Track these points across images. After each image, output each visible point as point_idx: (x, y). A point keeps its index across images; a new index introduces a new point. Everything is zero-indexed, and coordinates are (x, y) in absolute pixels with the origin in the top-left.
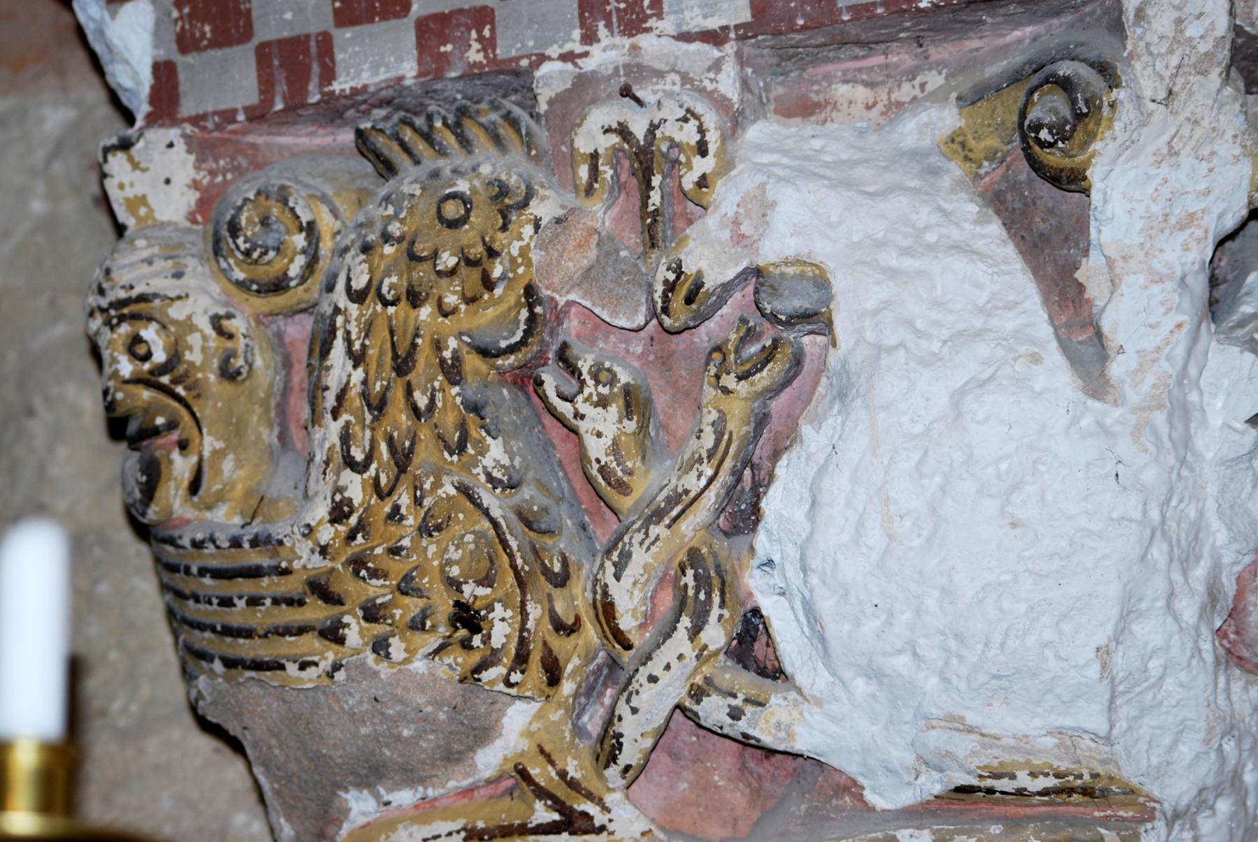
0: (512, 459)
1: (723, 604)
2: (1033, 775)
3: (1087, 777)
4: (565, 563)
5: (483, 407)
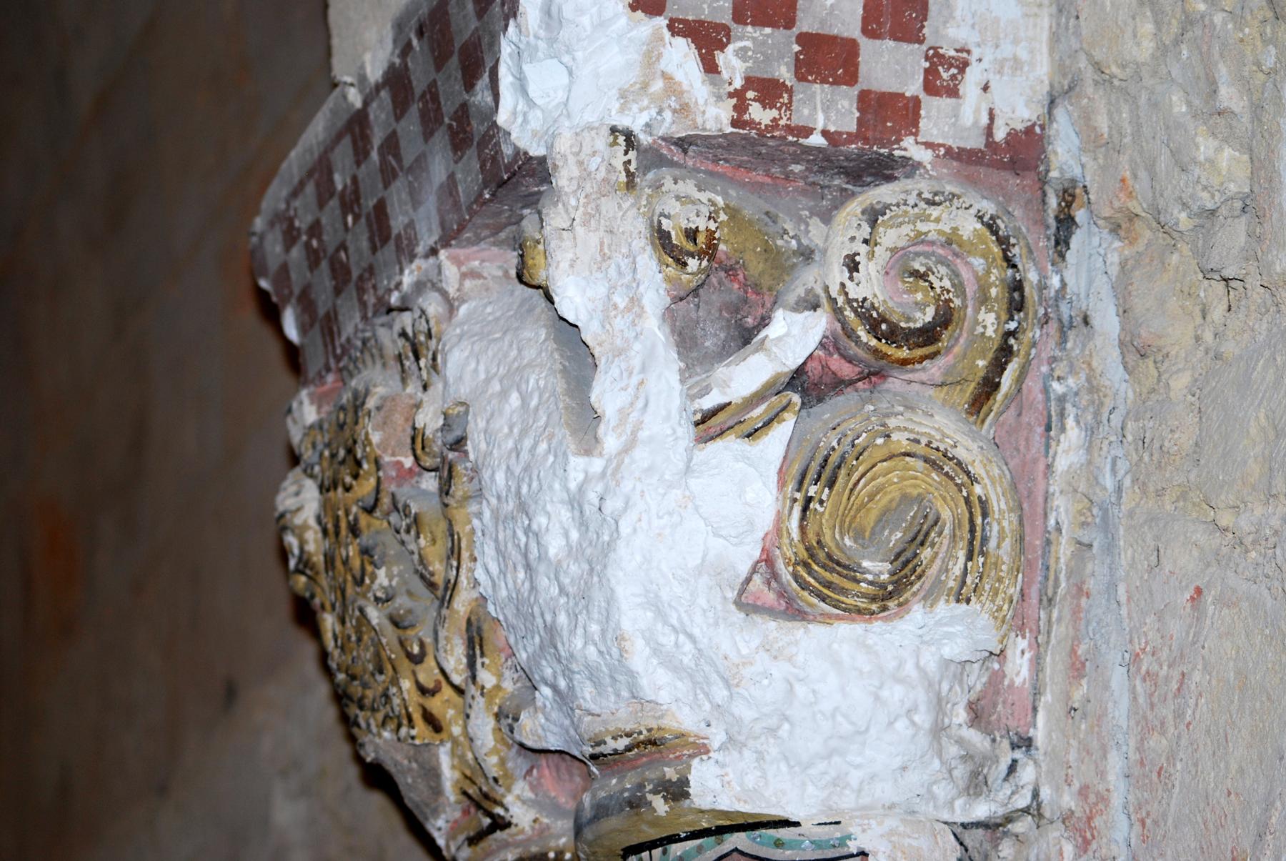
0: (390, 581)
1: (482, 655)
2: (614, 738)
3: (645, 732)
4: (422, 645)
5: (373, 548)
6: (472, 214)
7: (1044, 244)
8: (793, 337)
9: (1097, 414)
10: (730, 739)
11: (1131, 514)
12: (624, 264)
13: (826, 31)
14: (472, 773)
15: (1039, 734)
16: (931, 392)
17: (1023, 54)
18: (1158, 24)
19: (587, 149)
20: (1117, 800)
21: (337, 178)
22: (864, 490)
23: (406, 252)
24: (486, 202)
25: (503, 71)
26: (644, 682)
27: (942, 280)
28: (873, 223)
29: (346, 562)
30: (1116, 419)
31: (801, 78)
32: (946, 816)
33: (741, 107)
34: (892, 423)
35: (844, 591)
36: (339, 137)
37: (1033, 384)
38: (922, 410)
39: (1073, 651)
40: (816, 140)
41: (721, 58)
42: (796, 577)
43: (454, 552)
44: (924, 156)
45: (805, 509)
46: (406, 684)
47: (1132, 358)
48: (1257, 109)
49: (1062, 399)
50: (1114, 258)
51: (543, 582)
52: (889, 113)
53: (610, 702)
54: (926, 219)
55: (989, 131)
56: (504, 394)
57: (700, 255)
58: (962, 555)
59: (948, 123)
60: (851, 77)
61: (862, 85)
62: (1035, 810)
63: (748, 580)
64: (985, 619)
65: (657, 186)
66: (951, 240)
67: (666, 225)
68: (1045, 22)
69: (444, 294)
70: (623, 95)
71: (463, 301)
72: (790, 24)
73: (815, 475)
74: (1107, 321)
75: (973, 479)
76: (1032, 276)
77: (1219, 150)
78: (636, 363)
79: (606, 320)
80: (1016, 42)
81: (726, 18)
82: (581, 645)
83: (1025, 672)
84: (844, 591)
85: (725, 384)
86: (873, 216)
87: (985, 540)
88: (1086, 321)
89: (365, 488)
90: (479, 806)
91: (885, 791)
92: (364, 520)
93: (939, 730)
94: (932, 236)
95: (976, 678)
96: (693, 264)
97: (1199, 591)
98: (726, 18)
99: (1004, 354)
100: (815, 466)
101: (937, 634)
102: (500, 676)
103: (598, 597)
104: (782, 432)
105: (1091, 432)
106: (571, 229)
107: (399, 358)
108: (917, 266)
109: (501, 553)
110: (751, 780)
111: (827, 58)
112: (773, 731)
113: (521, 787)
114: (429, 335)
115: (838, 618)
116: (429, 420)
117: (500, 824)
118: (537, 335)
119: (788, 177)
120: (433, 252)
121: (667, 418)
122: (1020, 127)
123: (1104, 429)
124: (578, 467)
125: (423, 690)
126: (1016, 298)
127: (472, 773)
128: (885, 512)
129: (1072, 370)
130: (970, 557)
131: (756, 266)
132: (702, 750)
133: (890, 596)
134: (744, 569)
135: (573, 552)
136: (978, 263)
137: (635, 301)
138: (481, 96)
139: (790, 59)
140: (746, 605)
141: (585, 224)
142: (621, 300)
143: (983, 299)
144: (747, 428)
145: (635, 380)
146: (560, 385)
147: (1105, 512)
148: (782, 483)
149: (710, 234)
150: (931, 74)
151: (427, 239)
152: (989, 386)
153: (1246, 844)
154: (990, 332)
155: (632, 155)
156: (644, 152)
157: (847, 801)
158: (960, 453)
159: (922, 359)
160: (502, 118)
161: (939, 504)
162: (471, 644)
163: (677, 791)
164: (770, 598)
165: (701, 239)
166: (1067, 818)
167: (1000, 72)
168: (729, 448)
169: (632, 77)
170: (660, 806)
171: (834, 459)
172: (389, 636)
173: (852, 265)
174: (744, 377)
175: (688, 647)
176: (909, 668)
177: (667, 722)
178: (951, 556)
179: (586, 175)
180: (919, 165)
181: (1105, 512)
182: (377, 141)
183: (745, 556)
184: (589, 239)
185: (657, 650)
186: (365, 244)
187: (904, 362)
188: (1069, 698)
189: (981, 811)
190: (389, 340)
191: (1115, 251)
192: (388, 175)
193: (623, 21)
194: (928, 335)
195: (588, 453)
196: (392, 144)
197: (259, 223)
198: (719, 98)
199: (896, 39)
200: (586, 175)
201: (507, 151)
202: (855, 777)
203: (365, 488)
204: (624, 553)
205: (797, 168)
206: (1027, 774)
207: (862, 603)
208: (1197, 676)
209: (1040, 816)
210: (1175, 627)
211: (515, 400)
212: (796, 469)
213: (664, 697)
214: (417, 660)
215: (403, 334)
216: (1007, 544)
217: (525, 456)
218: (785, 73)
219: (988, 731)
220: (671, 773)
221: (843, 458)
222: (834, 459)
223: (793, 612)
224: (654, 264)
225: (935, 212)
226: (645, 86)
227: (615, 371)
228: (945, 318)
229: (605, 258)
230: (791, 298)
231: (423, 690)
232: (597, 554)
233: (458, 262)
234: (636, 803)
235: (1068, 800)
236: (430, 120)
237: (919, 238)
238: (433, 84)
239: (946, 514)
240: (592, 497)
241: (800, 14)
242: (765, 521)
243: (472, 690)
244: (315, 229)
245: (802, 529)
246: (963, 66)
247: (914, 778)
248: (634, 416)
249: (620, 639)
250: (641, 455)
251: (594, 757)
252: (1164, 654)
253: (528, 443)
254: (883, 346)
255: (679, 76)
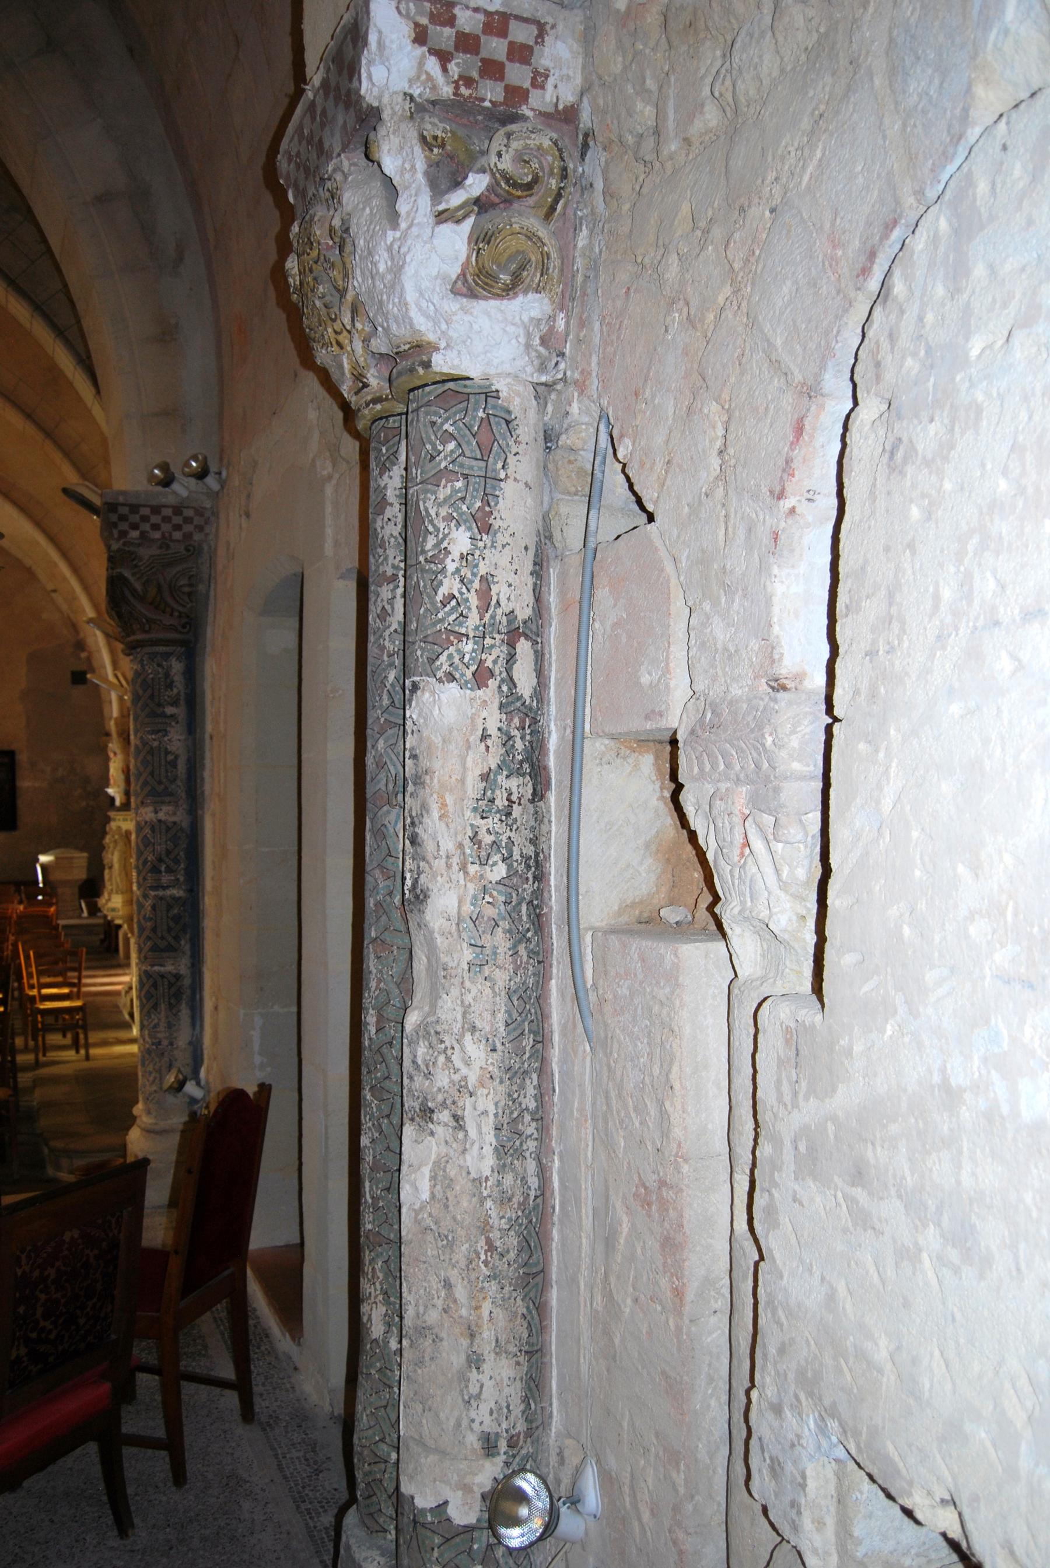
6: (353, 136)
7: (577, 154)
8: (476, 184)
9: (594, 224)
10: (448, 345)
11: (605, 261)
12: (409, 150)
13: (491, 58)
14: (356, 365)
15: (567, 351)
16: (529, 210)
17: (571, 73)
18: (624, 57)
19: (394, 102)
20: (594, 374)
21: (305, 131)
22: (501, 246)
23: (330, 158)
24: (357, 130)
25: (363, 70)
26: (415, 321)
27: (535, 165)
28: (508, 139)
29: (308, 283)
30: (601, 224)
31: (481, 77)
32: (530, 379)
33: (457, 88)
34: (513, 220)
35: (492, 287)
36: (305, 115)
37: (570, 212)
38: (525, 218)
39: (581, 318)
40: (487, 104)
41: (449, 67)
42: (474, 280)
43: (346, 276)
44: (529, 113)
45: (478, 253)
46: (330, 330)
47: (608, 198)
48: (661, 87)
49: (581, 218)
50: (603, 159)
51: (378, 283)
52: (516, 94)
53: (403, 331)
54: (529, 138)
55: (556, 105)
56: (364, 209)
57: (439, 147)
58: (538, 275)
59: (542, 100)
60: (502, 78)
61: (506, 82)
62: (564, 379)
63: (456, 282)
64: (546, 301)
65: (423, 119)
66: (539, 148)
67: (425, 133)
68: (580, 60)
69: (343, 172)
70: (410, 81)
71: (350, 175)
72: (477, 53)
73: (481, 239)
74: (599, 185)
75: (544, 245)
76: (571, 166)
77: (645, 107)
78: (413, 192)
79: (402, 174)
80: (568, 68)
81: (451, 49)
82: (392, 308)
83: (563, 327)
84: (492, 287)
85: (448, 202)
86: (508, 136)
87: (548, 269)
88: (591, 185)
89: (314, 254)
90: (358, 379)
91: (507, 368)
92: (314, 266)
93: (528, 346)
94: (532, 146)
95: (544, 328)
96: (436, 150)
97: (629, 289)
98: (451, 49)
99: (559, 196)
100: (482, 236)
101: (531, 306)
102: (364, 325)
103: (398, 288)
104: (470, 221)
105: (591, 231)
106: (388, 135)
107: (327, 201)
108: (526, 158)
109: (362, 273)
110: (456, 362)
111: (492, 69)
112: (464, 342)
113: (373, 371)
114: (337, 189)
115: (490, 298)
116: (336, 222)
117: (366, 385)
118: (377, 184)
119: (476, 121)
120: (339, 155)
121: (425, 215)
122: (569, 104)
123: (596, 228)
124: (391, 235)
125: (336, 332)
126: (564, 174)
127: (356, 365)
128: (510, 256)
129: (586, 206)
130: (542, 275)
131: (462, 156)
132: (437, 349)
133: (510, 289)
134: (454, 277)
135: (389, 270)
136: (550, 158)
137: (413, 167)
138: (355, 83)
139: (477, 69)
140: (455, 292)
141: (394, 133)
142: (407, 166)
143: (551, 174)
144: (455, 219)
145: (413, 199)
146: (385, 204)
147: (595, 262)
148: (469, 243)
149: (443, 139)
150: (534, 79)
151: (337, 150)
152: (552, 209)
153: (641, 385)
154: (553, 187)
155: (413, 105)
156: (417, 104)
157: (492, 371)
158: (540, 234)
159: (526, 196)
160: (363, 92)
161: (531, 254)
162: (352, 313)
163: (427, 365)
164: (465, 290)
165: (439, 140)
166: (576, 382)
167: (561, 80)
168: (447, 228)
169: (413, 73)
170: (421, 371)
171: (490, 233)
172: (323, 311)
173: (499, 155)
174: (456, 199)
175: (432, 308)
176: (517, 319)
177: (424, 338)
178: (534, 275)
179: (394, 113)
180: (528, 118)
181: (595, 262)
182: (318, 113)
183: (455, 271)
184: (395, 140)
185: (420, 309)
186: (315, 157)
187: (519, 197)
188: (578, 336)
189: (543, 379)
190: (324, 194)
191: (603, 157)
192: (323, 125)
193: (409, 48)
194: (529, 187)
195: (394, 229)
196: (324, 112)
197: (279, 157)
198: (448, 83)
199: (521, 63)
200: (394, 113)
201: (364, 105)
202: (496, 362)
203: (314, 254)
204: (409, 271)
205: (480, 118)
206: (562, 366)
207: (499, 291)
208: (626, 322)
209: (566, 381)
210: (619, 304)
211: (368, 211)
212: (475, 237)
213: (423, 328)
214: (334, 320)
215: (328, 190)
216: (556, 271)
217: (371, 232)
218: (475, 74)
219: (547, 347)
220: (425, 358)
221: (493, 233)
222: (490, 233)
223: (473, 295)
224: (420, 150)
225: (533, 136)
226: (419, 77)
227: (405, 196)
228: (536, 180)
229: (402, 148)
230: (475, 169)
231: (336, 332)
232: (397, 270)
233: (348, 159)
234: (412, 370)
235: (577, 376)
236: (337, 99)
237: (527, 147)
238: (338, 83)
239: (533, 259)
240: (396, 247)
241: (482, 50)
242: (463, 258)
243: (354, 331)
244: (298, 154)
245: (477, 261)
246: (547, 77)
247: (519, 363)
248: (413, 214)
249: (406, 304)
250: (415, 230)
251: (397, 353)
252: (614, 315)
253: (372, 227)
254: (511, 189)
255: (432, 73)
